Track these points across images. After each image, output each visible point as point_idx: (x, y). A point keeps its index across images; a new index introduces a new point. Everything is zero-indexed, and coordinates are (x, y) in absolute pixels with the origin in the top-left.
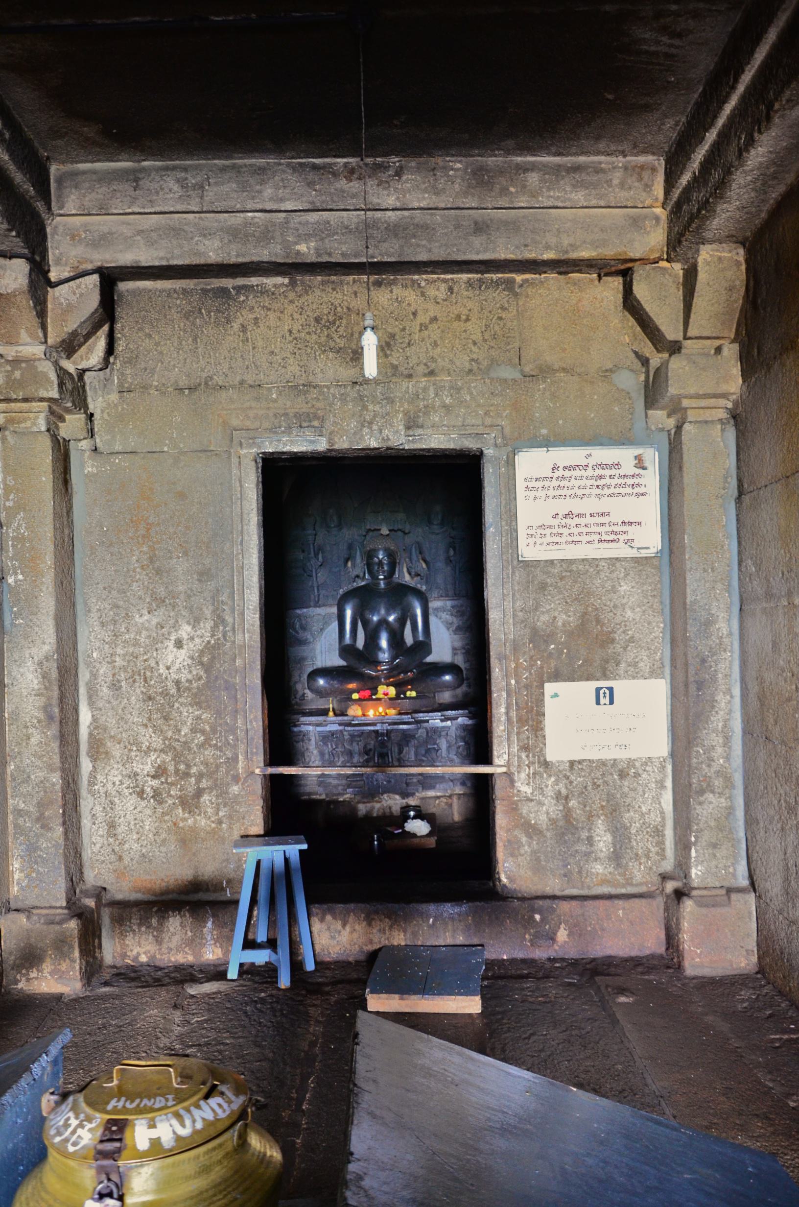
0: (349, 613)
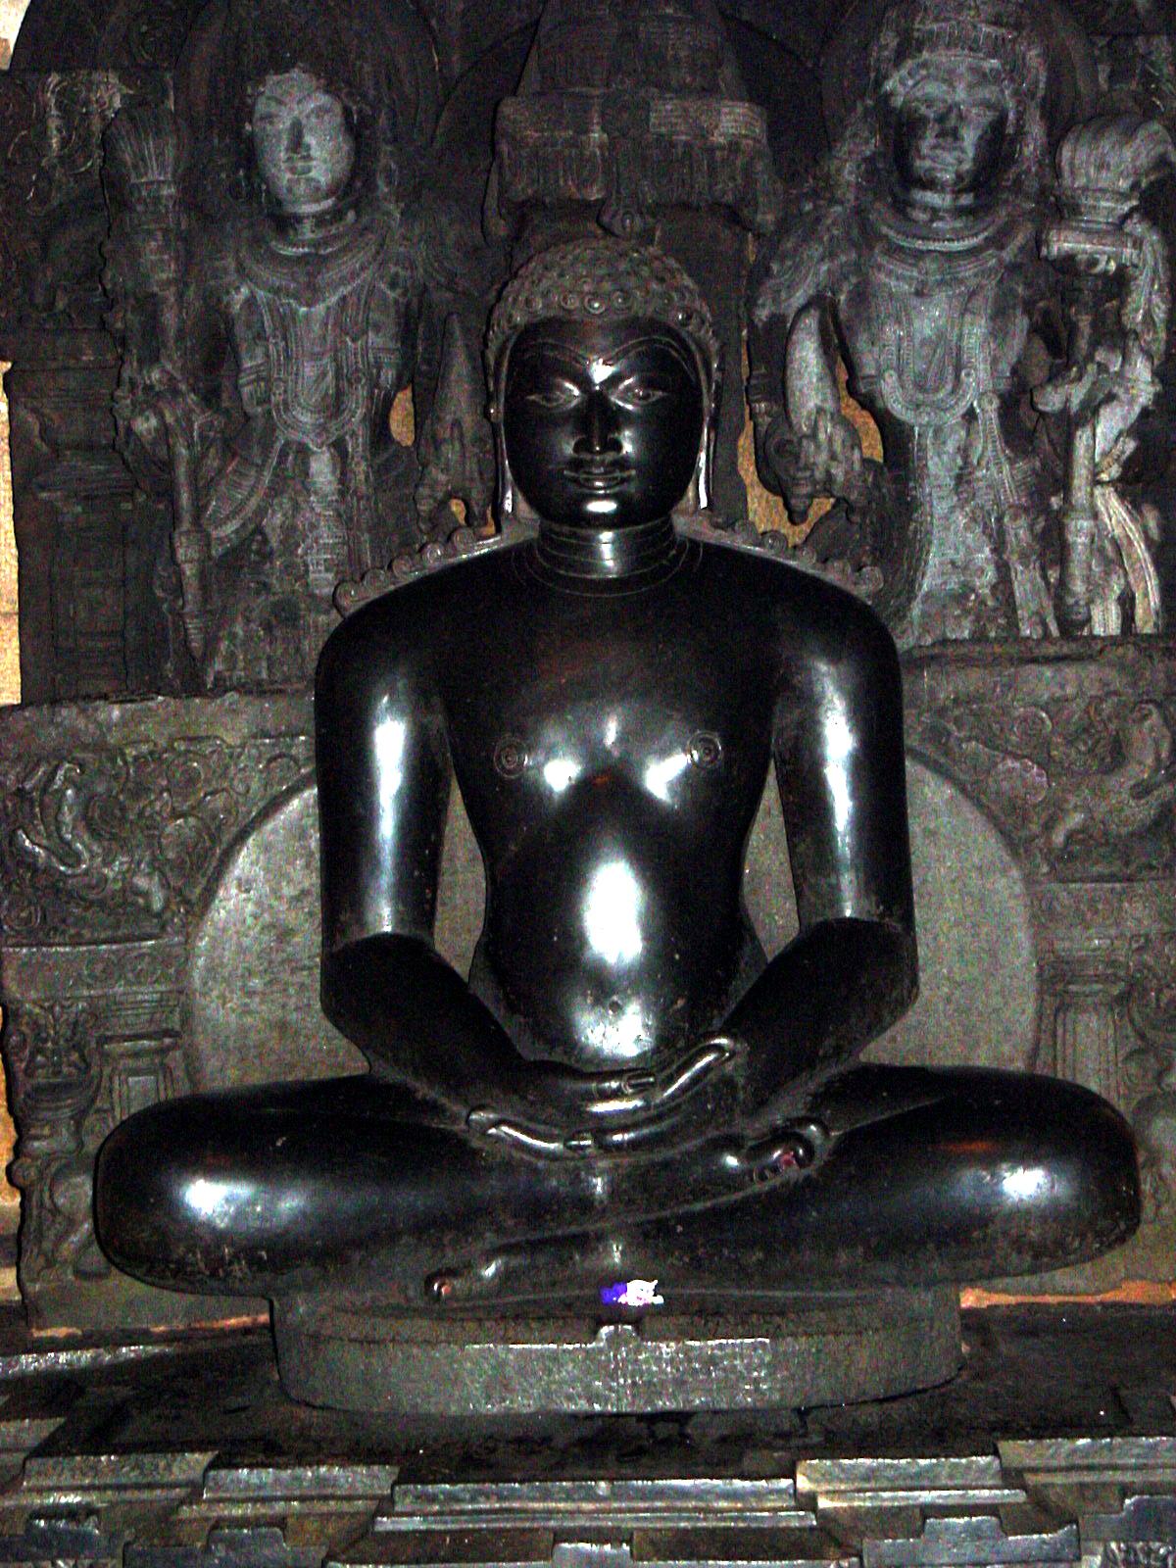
0: (390, 742)
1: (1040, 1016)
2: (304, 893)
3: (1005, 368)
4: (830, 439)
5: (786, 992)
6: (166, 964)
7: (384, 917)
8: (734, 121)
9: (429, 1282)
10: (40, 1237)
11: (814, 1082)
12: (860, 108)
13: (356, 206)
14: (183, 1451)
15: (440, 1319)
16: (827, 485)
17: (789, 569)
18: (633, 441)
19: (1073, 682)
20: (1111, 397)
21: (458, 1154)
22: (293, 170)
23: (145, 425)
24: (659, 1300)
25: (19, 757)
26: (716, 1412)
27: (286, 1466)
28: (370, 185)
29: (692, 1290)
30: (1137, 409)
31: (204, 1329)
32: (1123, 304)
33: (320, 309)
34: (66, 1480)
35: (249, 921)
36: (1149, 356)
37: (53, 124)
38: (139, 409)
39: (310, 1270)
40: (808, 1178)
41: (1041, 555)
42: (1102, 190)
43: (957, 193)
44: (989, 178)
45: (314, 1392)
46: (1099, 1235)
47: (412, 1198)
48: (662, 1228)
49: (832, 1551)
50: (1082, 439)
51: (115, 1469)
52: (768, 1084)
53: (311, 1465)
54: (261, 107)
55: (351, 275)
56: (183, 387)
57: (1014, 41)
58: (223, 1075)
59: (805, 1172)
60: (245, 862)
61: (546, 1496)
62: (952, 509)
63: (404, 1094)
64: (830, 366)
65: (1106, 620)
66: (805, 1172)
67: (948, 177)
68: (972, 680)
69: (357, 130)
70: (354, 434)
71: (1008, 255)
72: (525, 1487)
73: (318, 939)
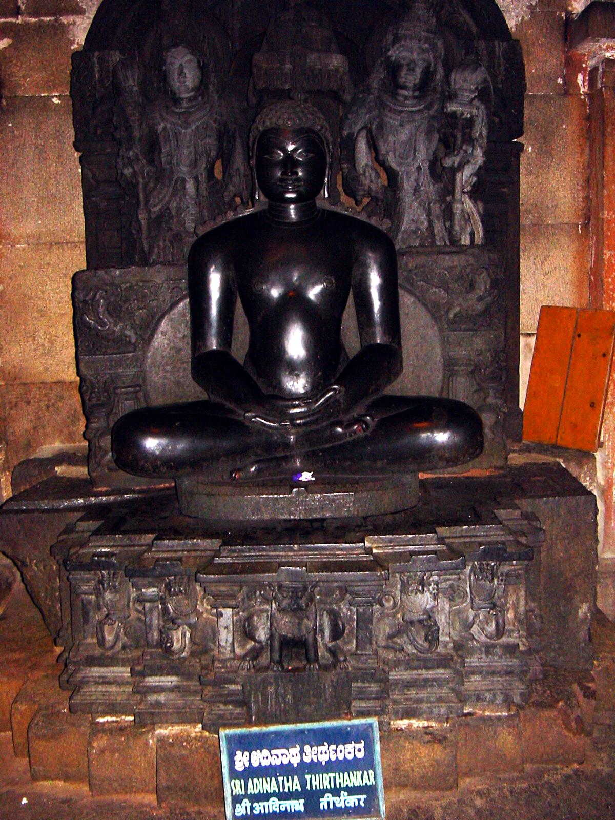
0: (215, 281)
1: (444, 377)
2: (185, 336)
3: (431, 152)
4: (370, 176)
5: (357, 368)
6: (137, 361)
7: (213, 344)
8: (336, 61)
9: (231, 473)
10: (96, 457)
11: (368, 401)
12: (379, 62)
13: (202, 95)
14: (145, 533)
15: (236, 486)
16: (369, 193)
17: (357, 219)
18: (302, 172)
19: (457, 261)
20: (468, 162)
21: (242, 428)
22: (180, 82)
23: (128, 171)
24: (314, 479)
25: (84, 288)
26: (334, 518)
27: (181, 539)
28: (207, 88)
29: (325, 475)
30: (477, 166)
31: (153, 489)
32: (472, 129)
33: (189, 130)
34: (104, 543)
35: (166, 346)
36: (482, 148)
37: (96, 69)
38: (125, 166)
39: (188, 470)
40: (367, 436)
41: (444, 218)
42: (466, 90)
43: (414, 91)
44: (424, 86)
45: (154, 788)
46: (470, 455)
47: (225, 444)
48: (314, 453)
49: (378, 568)
50: (458, 176)
51: (122, 540)
52: (353, 402)
53: (190, 539)
54: (169, 60)
55: (199, 119)
56: (141, 157)
57: (433, 38)
58: (158, 400)
59: (365, 433)
60: (164, 325)
61: (275, 551)
62: (412, 201)
63: (221, 407)
64: (370, 149)
65: (465, 240)
66: (365, 433)
67: (411, 85)
68: (422, 260)
69: (202, 68)
70: (201, 174)
71: (431, 112)
72: (268, 547)
73: (190, 352)
